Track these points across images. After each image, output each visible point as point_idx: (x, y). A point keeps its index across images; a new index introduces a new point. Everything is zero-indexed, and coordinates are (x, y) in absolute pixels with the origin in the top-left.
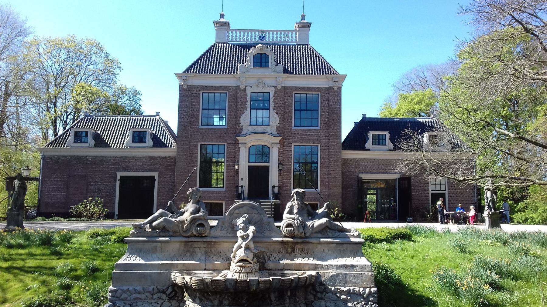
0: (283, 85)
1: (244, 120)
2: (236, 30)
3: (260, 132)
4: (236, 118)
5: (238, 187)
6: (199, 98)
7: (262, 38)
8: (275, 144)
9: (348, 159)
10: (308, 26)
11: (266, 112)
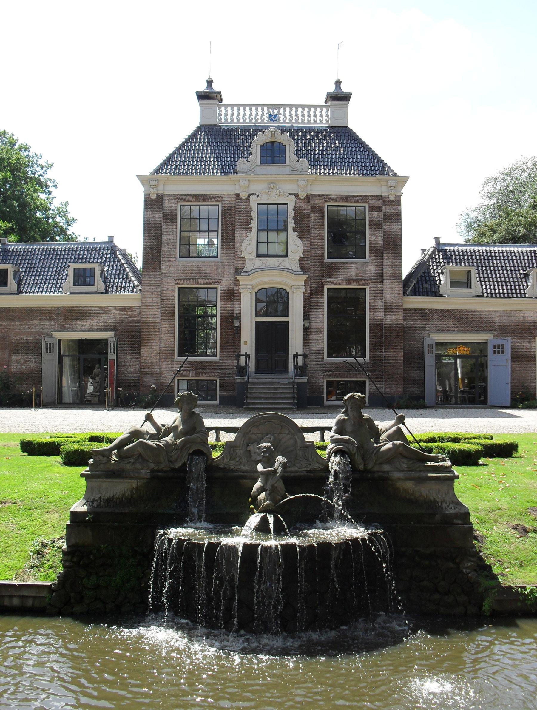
0: (309, 192)
1: (248, 247)
2: (232, 106)
3: (277, 268)
4: (234, 246)
5: (238, 355)
6: (176, 213)
7: (273, 118)
8: (299, 287)
9: (413, 310)
10: (346, 98)
11: (282, 237)
